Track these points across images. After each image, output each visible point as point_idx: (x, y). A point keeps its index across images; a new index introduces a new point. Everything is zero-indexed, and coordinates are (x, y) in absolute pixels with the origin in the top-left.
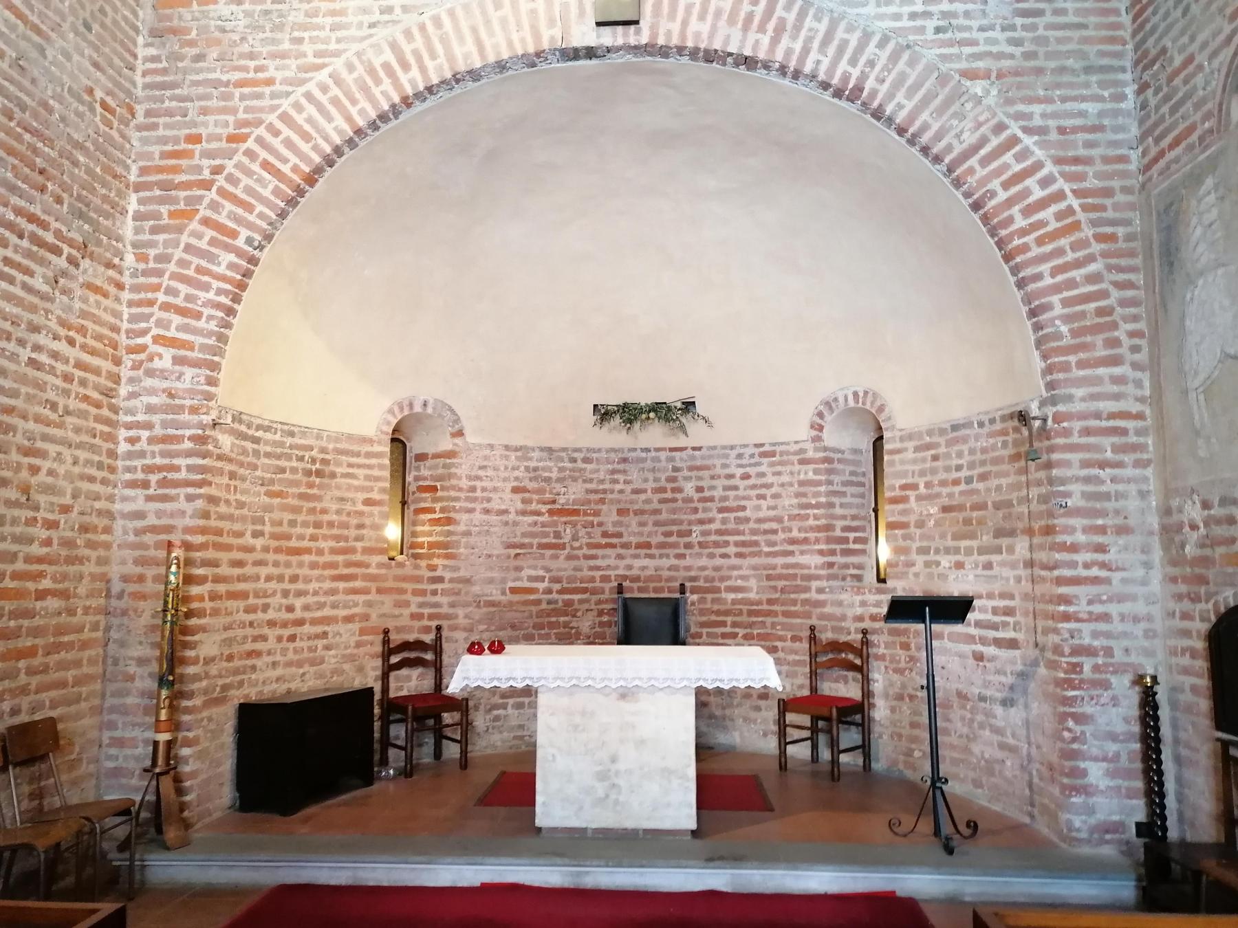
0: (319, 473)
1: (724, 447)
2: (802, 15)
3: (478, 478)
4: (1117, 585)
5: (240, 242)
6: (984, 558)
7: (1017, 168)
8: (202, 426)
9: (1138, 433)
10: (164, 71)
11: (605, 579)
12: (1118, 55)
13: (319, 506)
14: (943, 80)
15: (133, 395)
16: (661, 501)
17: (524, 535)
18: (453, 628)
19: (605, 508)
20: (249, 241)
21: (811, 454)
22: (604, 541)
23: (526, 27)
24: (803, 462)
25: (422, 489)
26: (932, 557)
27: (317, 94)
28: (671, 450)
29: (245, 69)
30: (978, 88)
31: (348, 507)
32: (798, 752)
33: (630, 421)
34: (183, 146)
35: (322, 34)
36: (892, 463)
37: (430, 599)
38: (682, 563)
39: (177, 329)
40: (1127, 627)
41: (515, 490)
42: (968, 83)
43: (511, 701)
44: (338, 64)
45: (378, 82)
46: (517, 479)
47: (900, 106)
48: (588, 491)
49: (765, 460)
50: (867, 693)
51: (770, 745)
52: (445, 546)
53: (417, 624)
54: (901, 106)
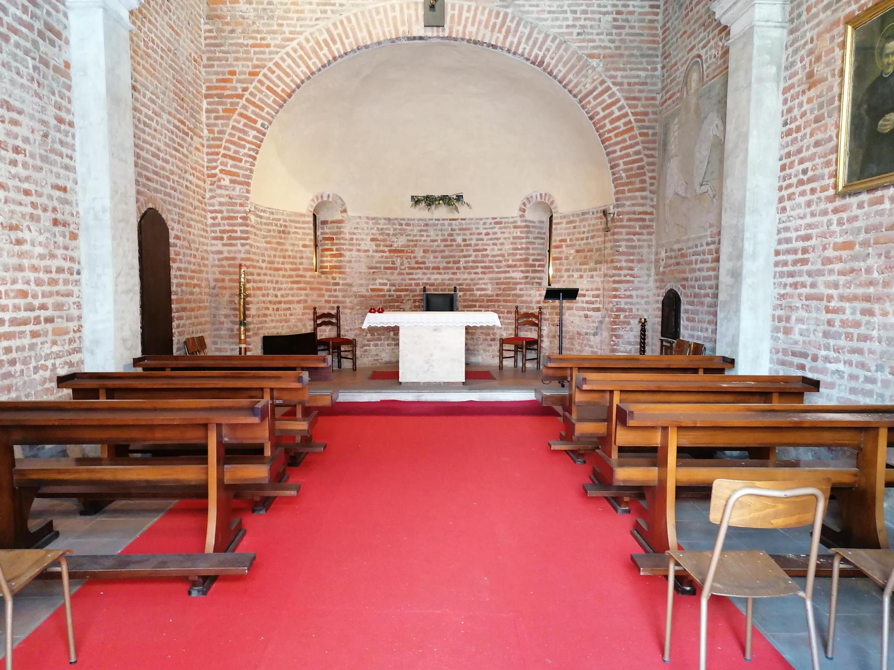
0: (284, 232)
1: (477, 219)
2: (518, 25)
3: (354, 234)
4: (636, 284)
5: (258, 125)
6: (591, 273)
7: (609, 101)
8: (245, 212)
9: (650, 220)
10: (215, 38)
11: (417, 285)
12: (655, 49)
13: (284, 247)
14: (579, 58)
15: (212, 197)
16: (445, 246)
17: (377, 262)
18: (345, 308)
19: (416, 249)
20: (263, 125)
21: (519, 224)
22: (416, 266)
23: (392, 25)
24: (515, 227)
25: (325, 239)
26: (571, 273)
27: (292, 53)
28: (451, 220)
29: (256, 38)
30: (594, 62)
31: (296, 248)
32: (508, 363)
33: (429, 205)
34: (227, 76)
35: (293, 22)
36: (556, 229)
37: (333, 293)
38: (455, 277)
39: (231, 167)
40: (639, 300)
41: (372, 240)
42: (590, 60)
43: (372, 343)
44: (301, 38)
45: (321, 49)
46: (373, 234)
47: (560, 71)
48: (408, 241)
49: (497, 226)
50: (540, 336)
51: (496, 361)
52: (339, 267)
53: (328, 305)
54: (561, 70)
